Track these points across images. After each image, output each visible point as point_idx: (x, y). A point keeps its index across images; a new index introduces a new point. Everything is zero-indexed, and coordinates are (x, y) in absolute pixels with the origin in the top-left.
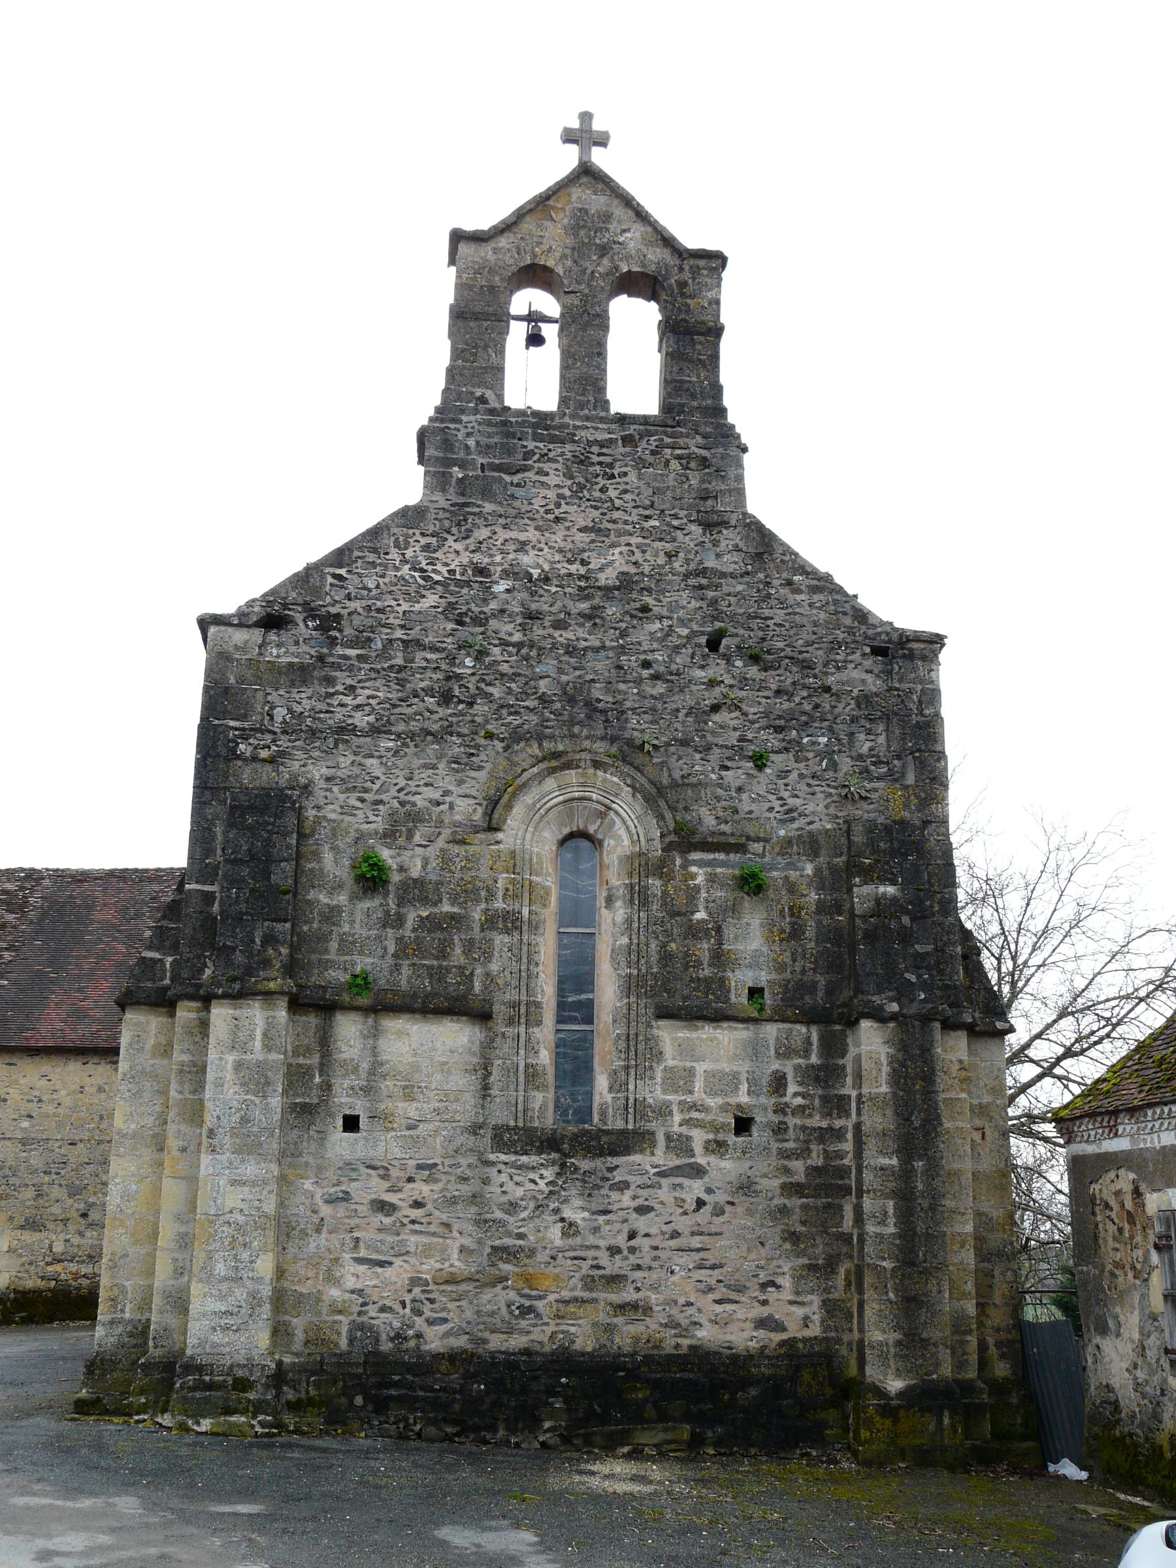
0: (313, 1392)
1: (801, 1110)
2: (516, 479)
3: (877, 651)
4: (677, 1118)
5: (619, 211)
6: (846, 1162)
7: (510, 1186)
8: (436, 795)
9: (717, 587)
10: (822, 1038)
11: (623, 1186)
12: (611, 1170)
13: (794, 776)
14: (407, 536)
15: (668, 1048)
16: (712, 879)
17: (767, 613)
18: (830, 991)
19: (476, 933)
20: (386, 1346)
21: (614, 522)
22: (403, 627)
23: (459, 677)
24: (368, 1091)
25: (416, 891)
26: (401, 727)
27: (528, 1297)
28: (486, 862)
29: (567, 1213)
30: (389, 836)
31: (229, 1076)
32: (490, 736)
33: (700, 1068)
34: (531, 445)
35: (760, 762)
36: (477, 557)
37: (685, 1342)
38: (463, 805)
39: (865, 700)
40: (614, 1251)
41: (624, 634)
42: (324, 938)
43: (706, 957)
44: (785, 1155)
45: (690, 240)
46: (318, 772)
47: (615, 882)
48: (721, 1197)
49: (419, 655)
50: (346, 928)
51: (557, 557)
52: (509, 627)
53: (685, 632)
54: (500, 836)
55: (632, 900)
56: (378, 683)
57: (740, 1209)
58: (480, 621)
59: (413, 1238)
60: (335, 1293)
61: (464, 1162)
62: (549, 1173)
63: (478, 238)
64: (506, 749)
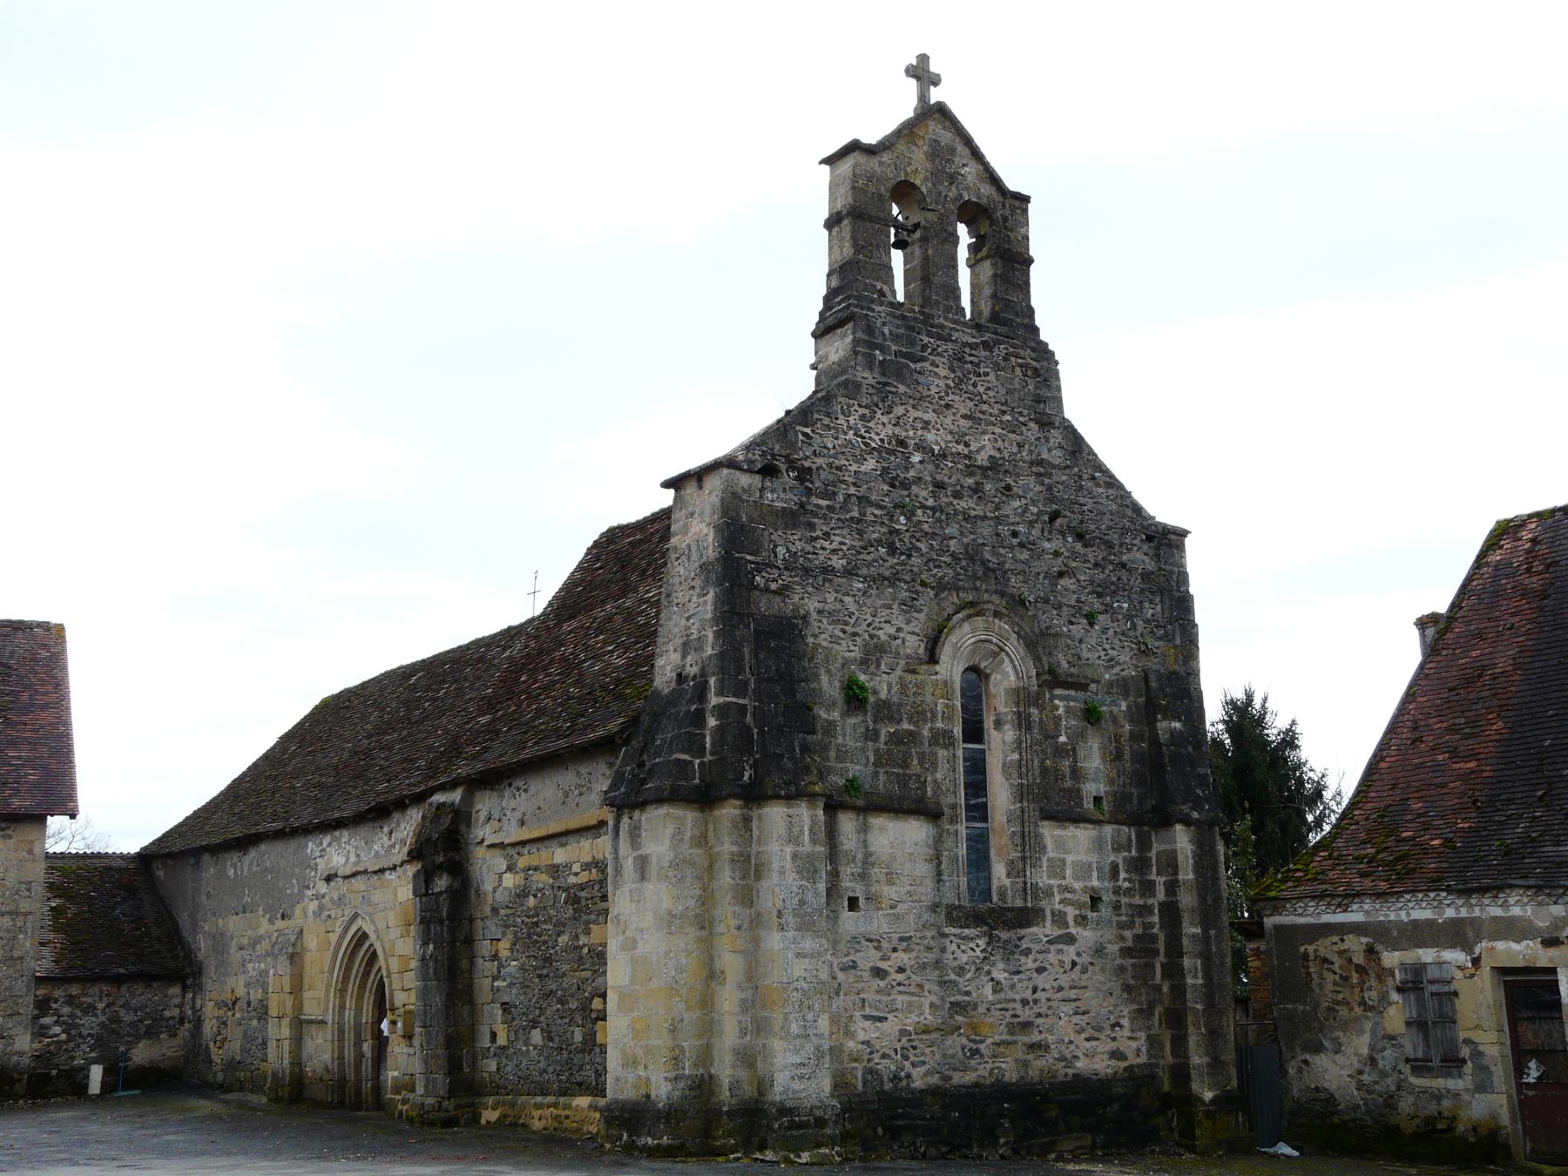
0: (848, 1126)
1: (1128, 891)
2: (918, 366)
3: (1150, 539)
4: (1057, 898)
5: (961, 148)
6: (1155, 930)
7: (958, 954)
8: (892, 631)
9: (1050, 475)
10: (1137, 836)
11: (1027, 952)
12: (1020, 939)
13: (1111, 632)
14: (849, 406)
15: (1049, 843)
16: (1068, 710)
17: (1082, 500)
18: (1141, 800)
19: (926, 748)
20: (888, 1086)
21: (983, 413)
22: (855, 484)
23: (898, 532)
24: (863, 877)
25: (886, 711)
26: (864, 571)
27: (974, 1041)
28: (929, 689)
29: (995, 974)
30: (864, 663)
31: (788, 864)
32: (923, 584)
33: (1070, 859)
34: (926, 340)
35: (1091, 619)
36: (897, 430)
37: (1070, 1071)
38: (911, 639)
39: (1146, 576)
40: (1025, 1002)
41: (997, 508)
42: (825, 748)
43: (1067, 771)
44: (1121, 926)
45: (1012, 184)
46: (812, 605)
47: (1002, 709)
48: (1086, 959)
49: (869, 510)
50: (840, 740)
51: (949, 438)
52: (924, 493)
53: (1035, 510)
54: (937, 668)
55: (1020, 725)
56: (845, 532)
57: (1097, 968)
58: (906, 485)
59: (900, 998)
60: (851, 1044)
61: (929, 934)
62: (982, 942)
63: (870, 150)
64: (936, 595)
